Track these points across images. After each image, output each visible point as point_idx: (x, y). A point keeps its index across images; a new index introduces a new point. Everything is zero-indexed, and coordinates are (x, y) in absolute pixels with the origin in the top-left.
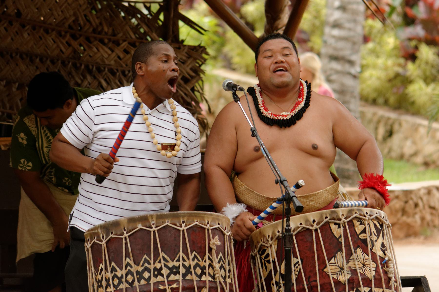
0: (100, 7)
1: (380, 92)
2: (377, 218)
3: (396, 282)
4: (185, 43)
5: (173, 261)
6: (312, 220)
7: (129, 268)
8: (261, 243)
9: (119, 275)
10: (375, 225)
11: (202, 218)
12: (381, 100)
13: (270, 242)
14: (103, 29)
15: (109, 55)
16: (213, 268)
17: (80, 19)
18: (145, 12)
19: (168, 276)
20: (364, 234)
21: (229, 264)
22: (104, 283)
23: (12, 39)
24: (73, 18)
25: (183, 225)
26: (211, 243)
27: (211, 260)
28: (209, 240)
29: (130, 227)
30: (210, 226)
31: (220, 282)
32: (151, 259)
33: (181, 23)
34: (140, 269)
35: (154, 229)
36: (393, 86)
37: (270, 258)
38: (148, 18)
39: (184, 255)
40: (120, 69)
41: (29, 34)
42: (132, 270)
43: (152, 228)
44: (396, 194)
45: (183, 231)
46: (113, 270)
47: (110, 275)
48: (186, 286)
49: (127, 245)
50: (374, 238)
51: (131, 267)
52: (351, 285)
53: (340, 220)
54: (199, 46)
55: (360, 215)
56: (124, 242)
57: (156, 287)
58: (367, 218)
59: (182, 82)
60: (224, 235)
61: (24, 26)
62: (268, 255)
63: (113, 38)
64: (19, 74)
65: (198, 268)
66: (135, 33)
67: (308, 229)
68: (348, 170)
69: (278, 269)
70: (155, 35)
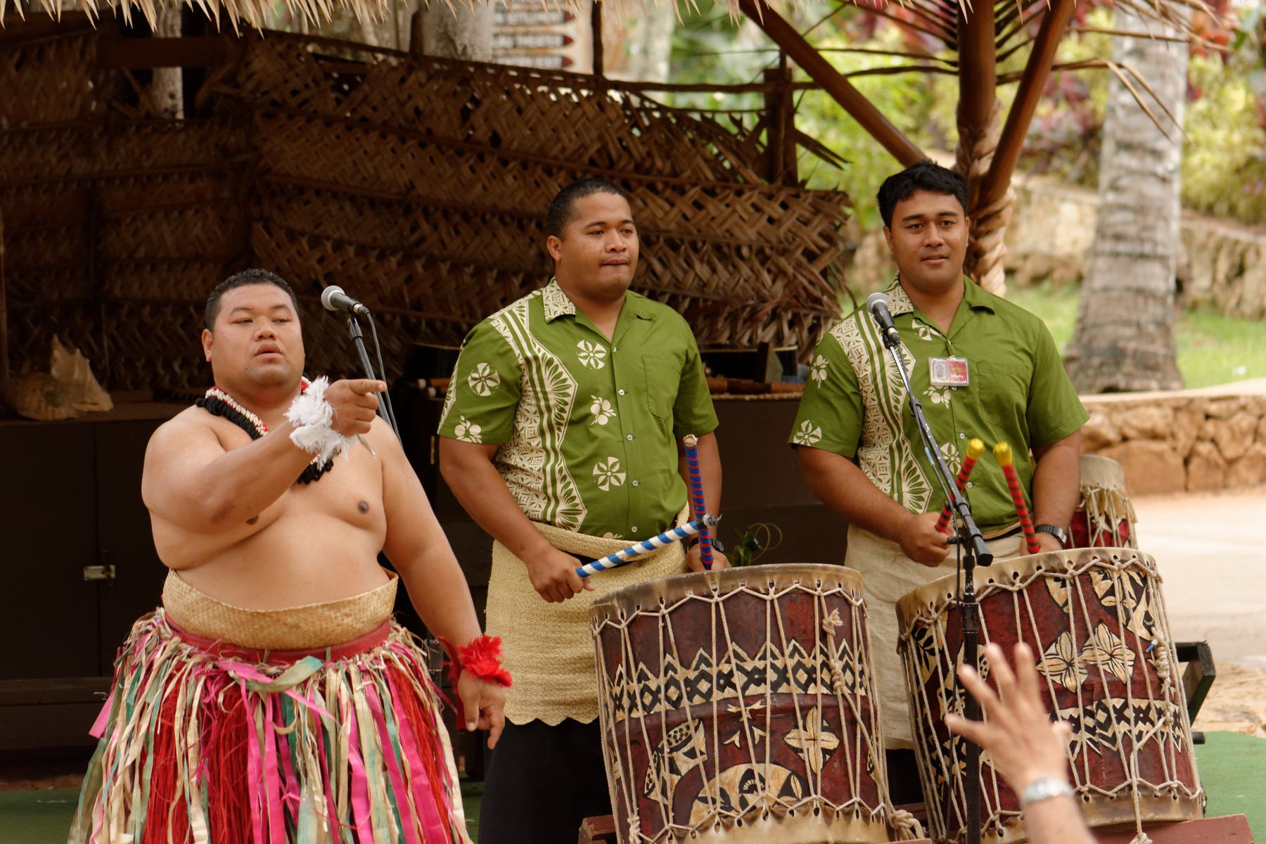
0: (647, 122)
1: (1219, 192)
2: (1134, 565)
3: (1173, 685)
4: (809, 186)
5: (753, 659)
6: (1012, 573)
7: (671, 673)
8: (917, 616)
9: (654, 688)
10: (1131, 579)
11: (809, 575)
12: (1222, 208)
13: (935, 615)
14: (653, 164)
15: (667, 213)
16: (830, 670)
17: (611, 146)
18: (734, 130)
19: (745, 688)
20: (1111, 598)
21: (860, 661)
22: (626, 702)
23: (484, 187)
24: (597, 145)
25: (772, 591)
26: (825, 622)
27: (827, 656)
28: (822, 617)
29: (672, 597)
30: (823, 591)
31: (843, 695)
32: (711, 656)
33: (801, 151)
34: (692, 675)
35: (716, 599)
36: (1243, 182)
37: (935, 645)
38: (738, 142)
39: (774, 648)
40: (687, 238)
41: (515, 178)
42: (677, 677)
43: (712, 597)
44: (1242, 402)
45: (772, 601)
46: (642, 677)
47: (636, 687)
48: (778, 705)
49: (666, 629)
50: (1131, 603)
51: (676, 672)
52: (1088, 696)
53: (1065, 571)
54: (835, 192)
55: (1103, 561)
56: (661, 624)
57: (723, 709)
58: (1115, 567)
59: (804, 260)
60: (850, 605)
61: (505, 163)
62: (930, 640)
63: (673, 181)
64: (498, 253)
65: (801, 671)
66: (714, 170)
67: (1005, 591)
68: (1155, 355)
69: (951, 667)
70: (751, 174)
